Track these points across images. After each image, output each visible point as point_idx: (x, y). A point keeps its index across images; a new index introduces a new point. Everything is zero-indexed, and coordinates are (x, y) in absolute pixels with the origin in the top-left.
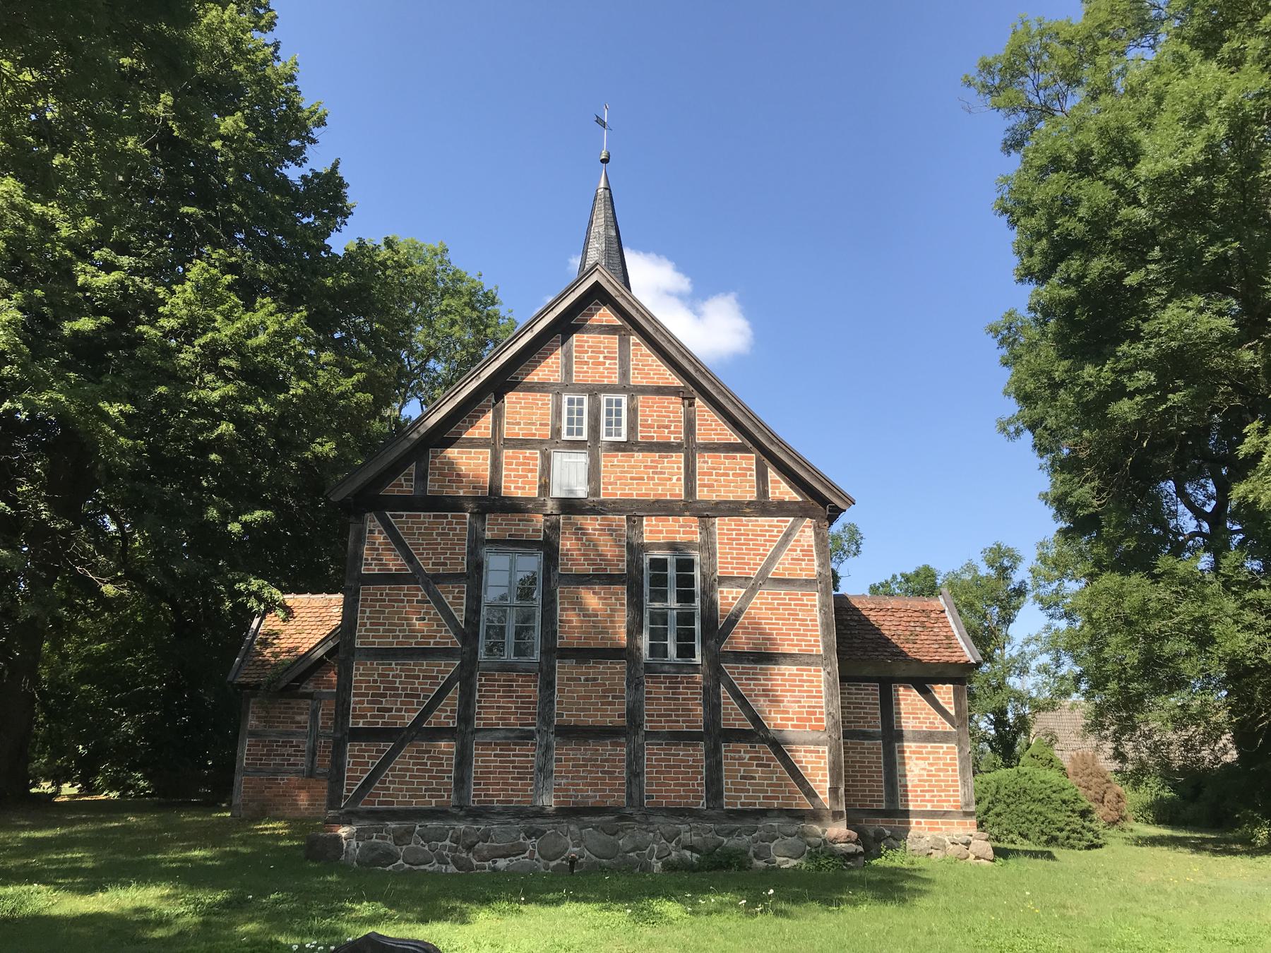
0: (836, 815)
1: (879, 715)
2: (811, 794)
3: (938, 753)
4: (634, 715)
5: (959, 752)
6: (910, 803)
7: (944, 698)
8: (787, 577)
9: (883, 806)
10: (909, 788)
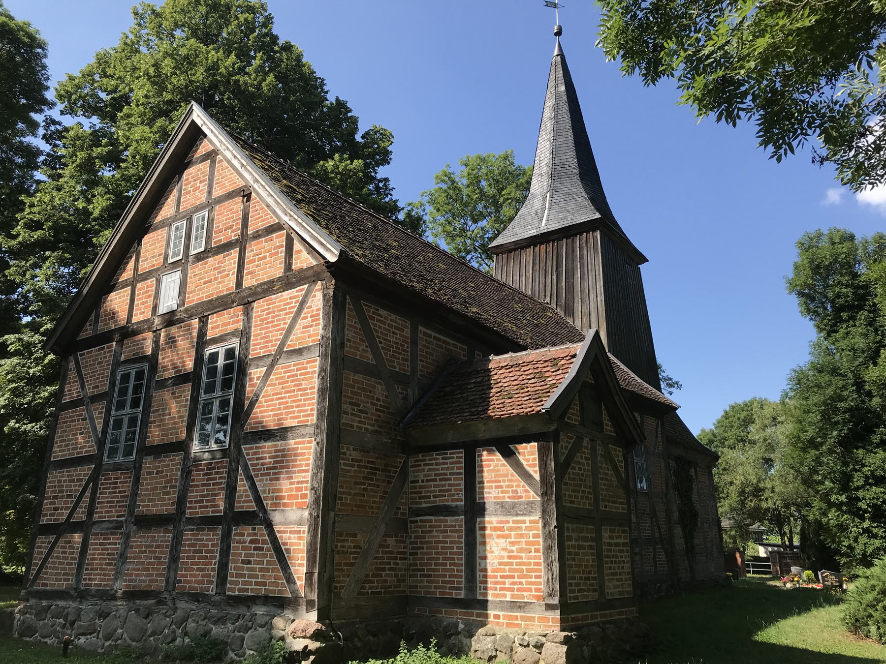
0: (310, 604)
1: (462, 487)
2: (290, 580)
3: (520, 528)
4: (181, 502)
5: (544, 527)
6: (490, 592)
7: (528, 460)
8: (298, 347)
9: (462, 595)
10: (489, 573)
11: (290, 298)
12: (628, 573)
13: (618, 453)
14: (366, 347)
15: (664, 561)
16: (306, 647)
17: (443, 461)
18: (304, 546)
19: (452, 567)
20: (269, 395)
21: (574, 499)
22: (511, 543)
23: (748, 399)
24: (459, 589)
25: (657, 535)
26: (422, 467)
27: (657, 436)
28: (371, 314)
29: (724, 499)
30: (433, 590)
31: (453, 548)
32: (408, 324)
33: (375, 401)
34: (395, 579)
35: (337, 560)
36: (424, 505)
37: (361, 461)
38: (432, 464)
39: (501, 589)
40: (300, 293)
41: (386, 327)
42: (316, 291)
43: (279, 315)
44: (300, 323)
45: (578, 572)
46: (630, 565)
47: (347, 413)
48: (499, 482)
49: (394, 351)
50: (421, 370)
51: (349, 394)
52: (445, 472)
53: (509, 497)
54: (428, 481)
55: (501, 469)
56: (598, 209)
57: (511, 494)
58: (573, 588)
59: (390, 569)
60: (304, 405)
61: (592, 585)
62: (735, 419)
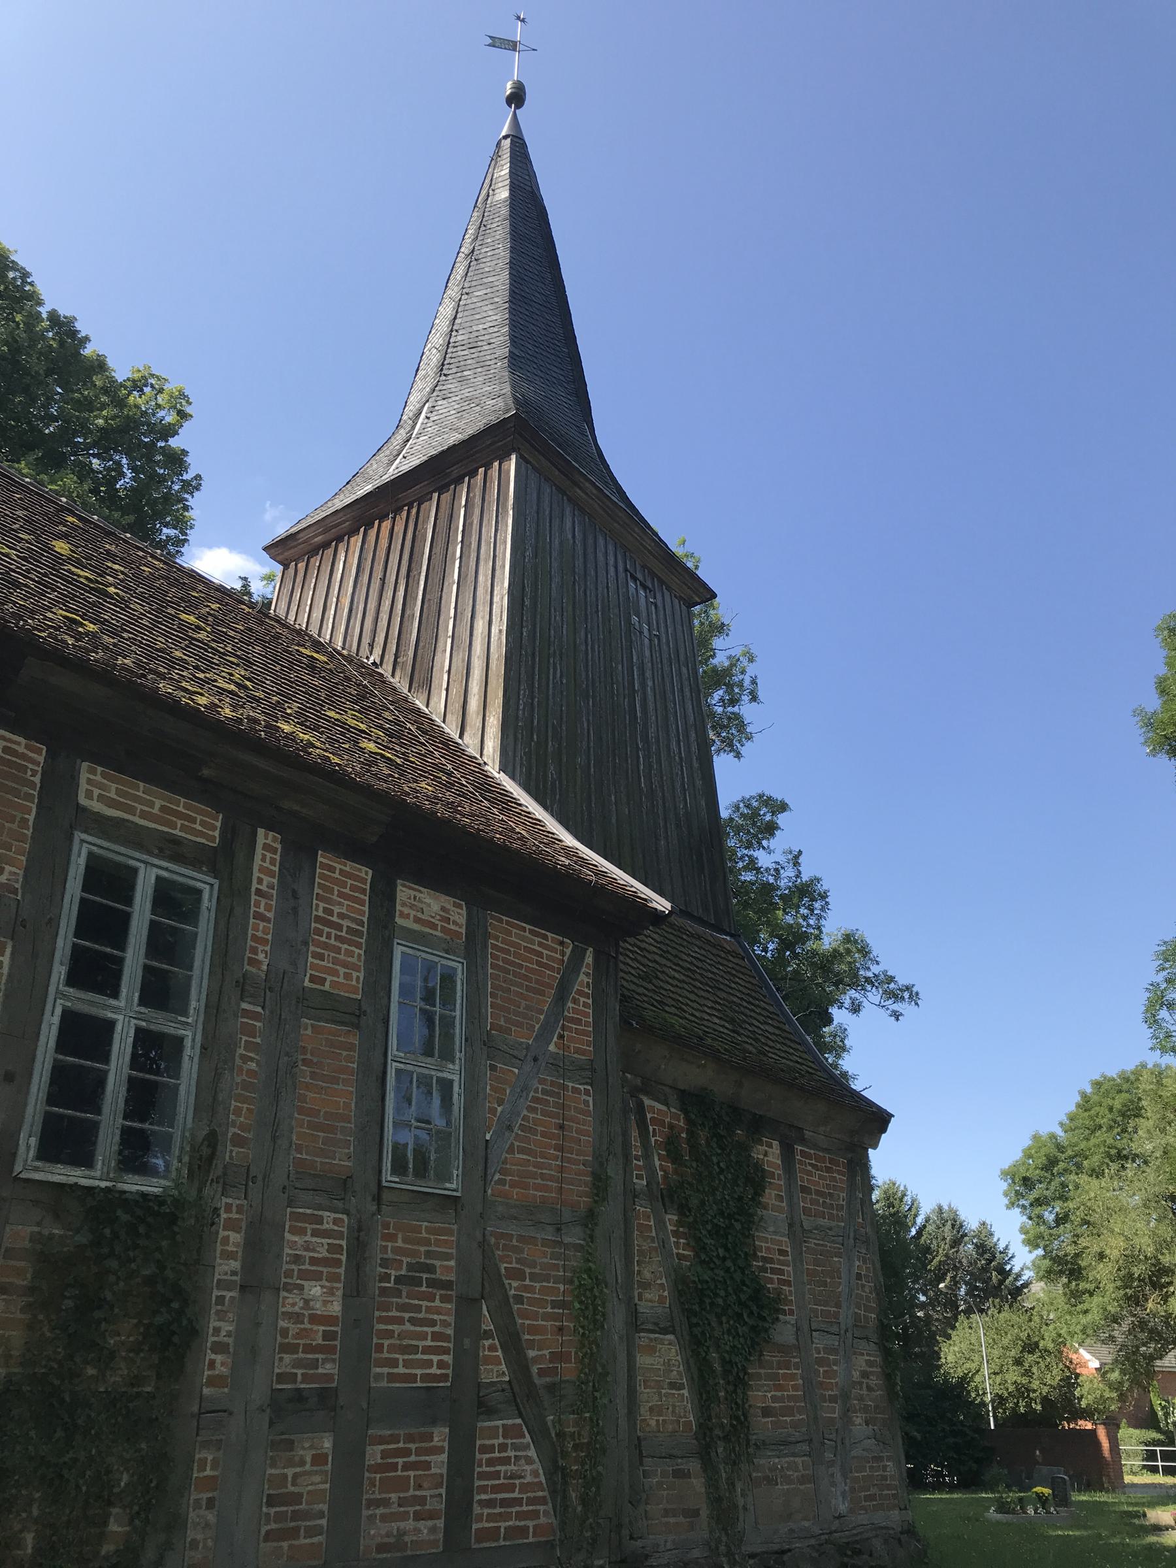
23: (1130, 1066)
29: (1091, 1295)
62: (1104, 1111)
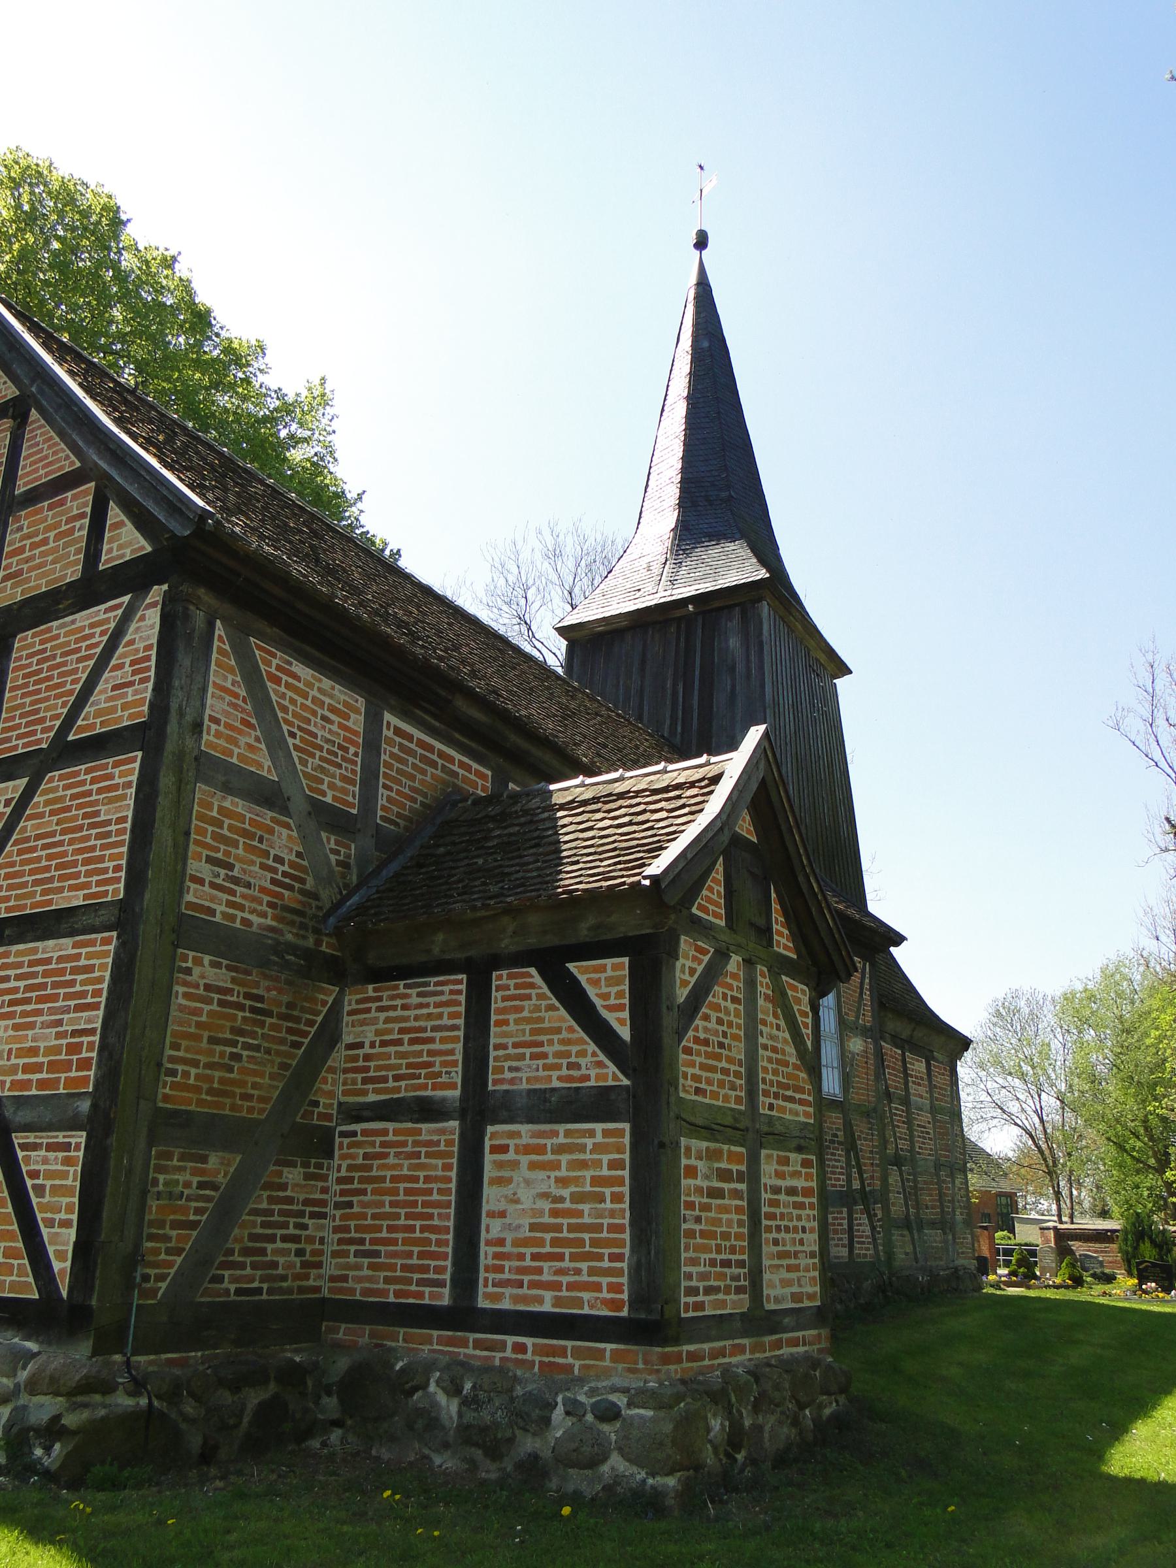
1: (459, 1057)
3: (582, 1148)
9: (444, 1298)
11: (92, 626)
12: (812, 1255)
13: (799, 994)
14: (257, 739)
15: (867, 1237)
16: (56, 1418)
17: (421, 1000)
18: (75, 1180)
19: (426, 1235)
20: (27, 840)
21: (703, 1086)
22: (558, 1180)
24: (441, 1284)
25: (856, 1185)
26: (373, 1014)
27: (861, 993)
28: (273, 670)
30: (381, 1286)
31: (429, 1192)
32: (361, 703)
33: (270, 862)
34: (298, 1260)
35: (153, 1213)
36: (372, 1098)
37: (229, 991)
38: (394, 1008)
39: (533, 1285)
40: (112, 614)
41: (309, 703)
42: (147, 608)
43: (64, 664)
44: (109, 678)
45: (706, 1249)
46: (816, 1236)
47: (201, 882)
48: (541, 1044)
49: (322, 759)
50: (384, 808)
51: (209, 840)
52: (422, 1023)
53: (559, 1078)
54: (384, 1044)
55: (547, 1015)
56: (763, 562)
57: (564, 1072)
58: (694, 1283)
59: (285, 1239)
60: (101, 859)
61: (736, 1278)
